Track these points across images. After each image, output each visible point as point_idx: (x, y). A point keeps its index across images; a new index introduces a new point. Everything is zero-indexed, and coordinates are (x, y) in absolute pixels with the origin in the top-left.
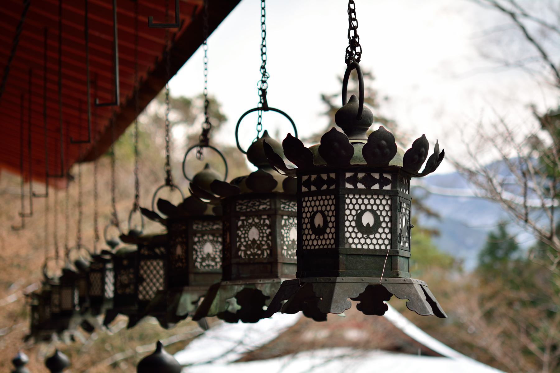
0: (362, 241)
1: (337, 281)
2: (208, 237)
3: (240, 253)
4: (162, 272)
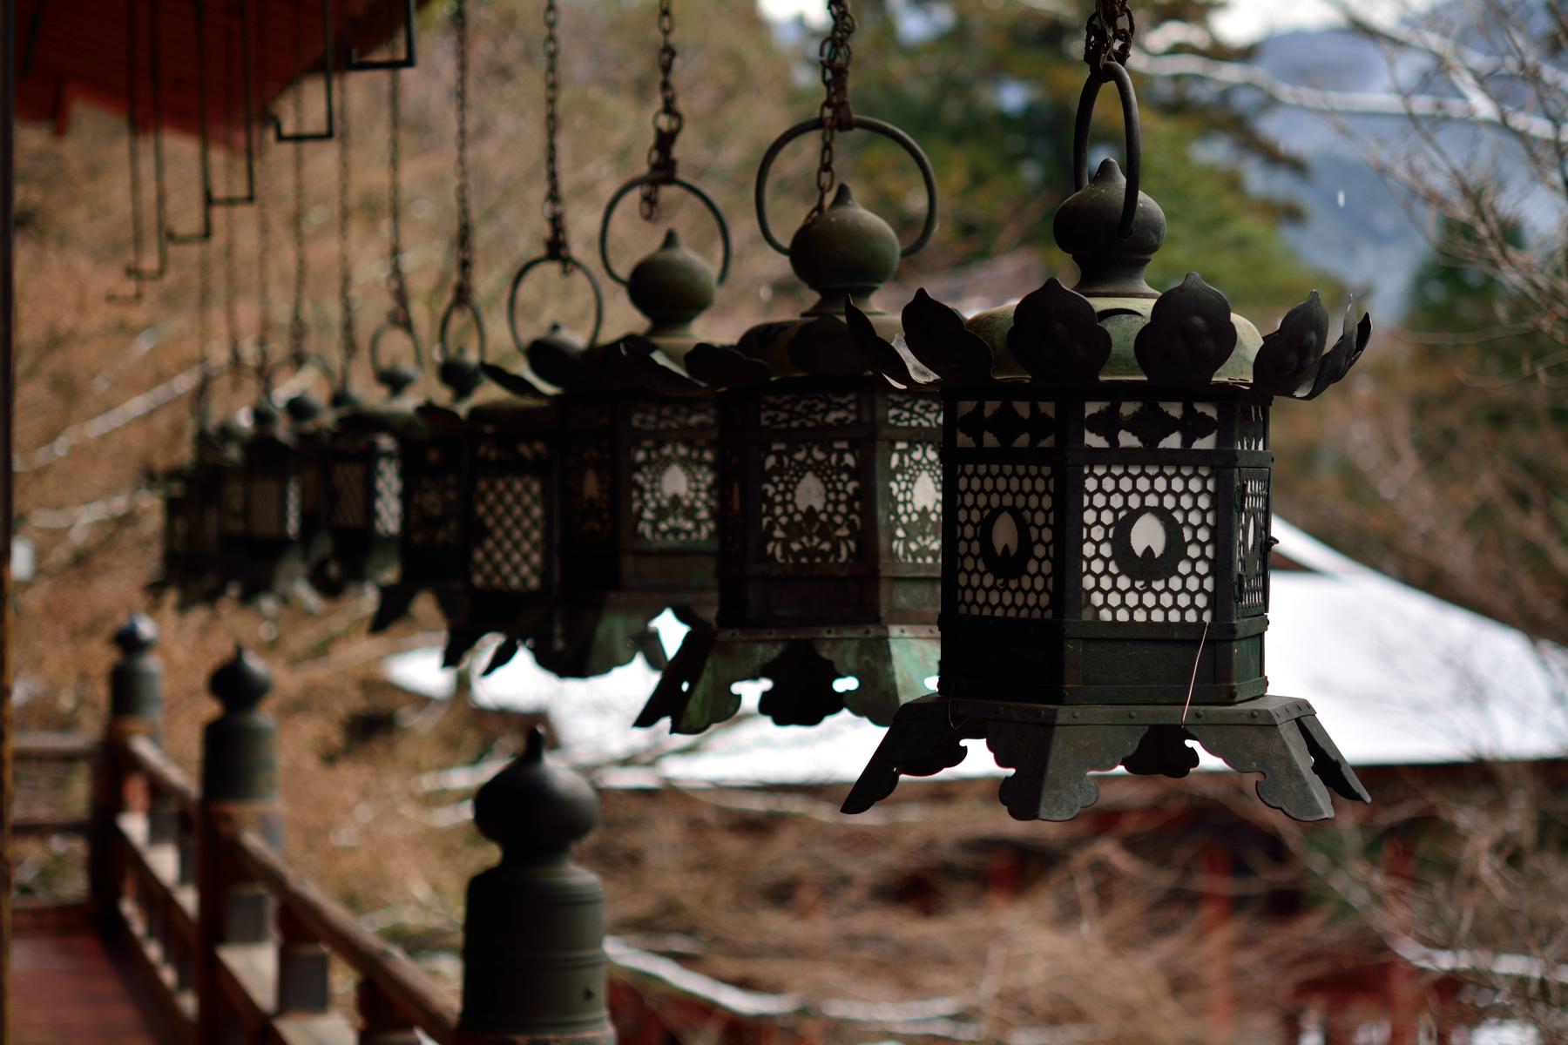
0: (1132, 599)
1: (1059, 721)
2: (675, 450)
3: (770, 547)
4: (537, 512)
